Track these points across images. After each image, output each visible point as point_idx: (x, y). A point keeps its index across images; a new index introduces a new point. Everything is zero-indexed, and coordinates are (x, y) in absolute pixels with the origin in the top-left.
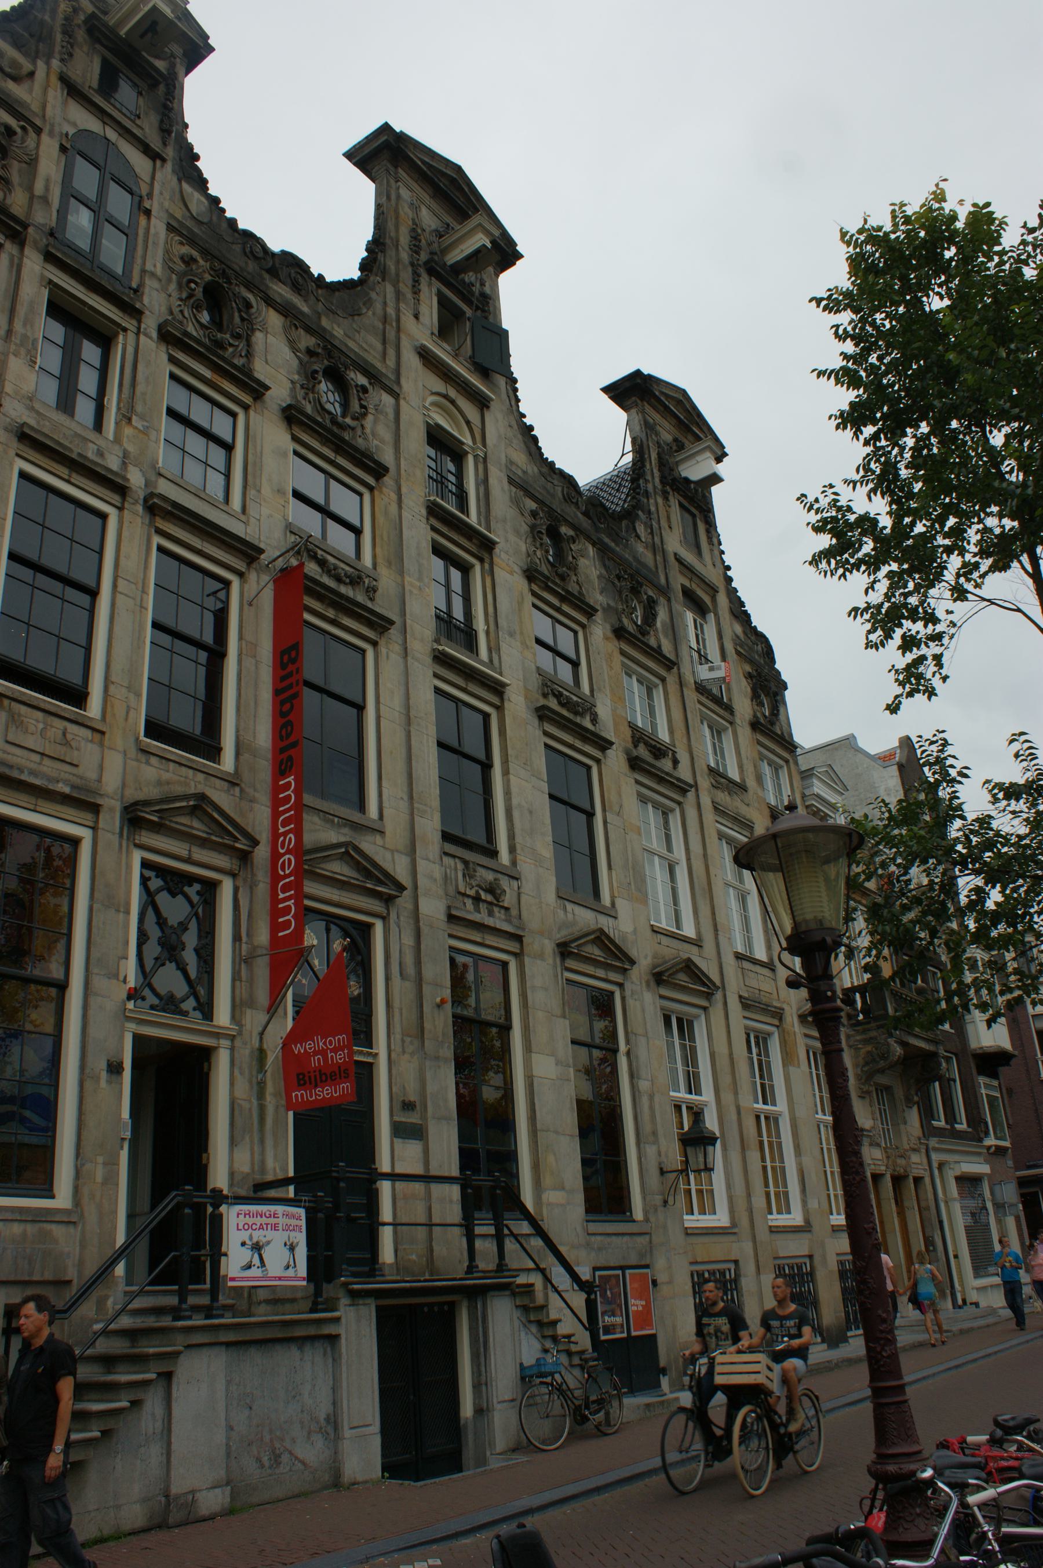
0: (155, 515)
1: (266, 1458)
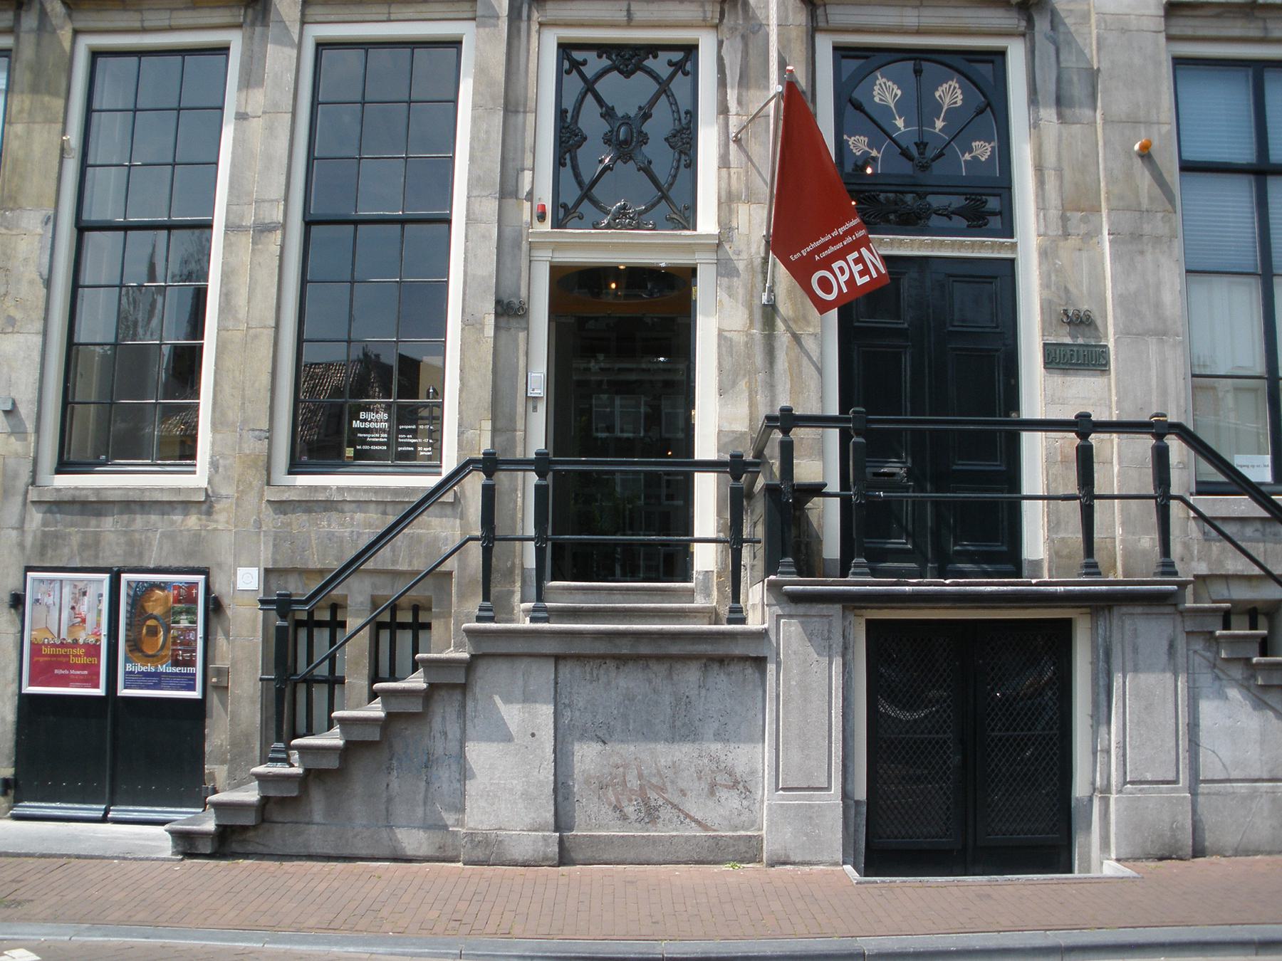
1: (631, 809)
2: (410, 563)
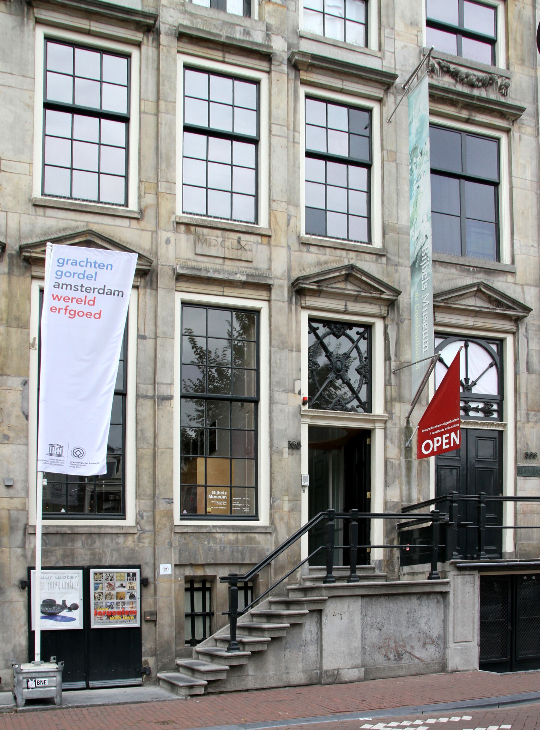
0: (299, 70)
1: (392, 655)
2: (251, 560)
